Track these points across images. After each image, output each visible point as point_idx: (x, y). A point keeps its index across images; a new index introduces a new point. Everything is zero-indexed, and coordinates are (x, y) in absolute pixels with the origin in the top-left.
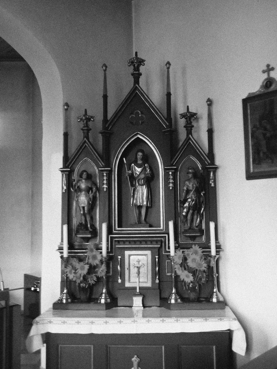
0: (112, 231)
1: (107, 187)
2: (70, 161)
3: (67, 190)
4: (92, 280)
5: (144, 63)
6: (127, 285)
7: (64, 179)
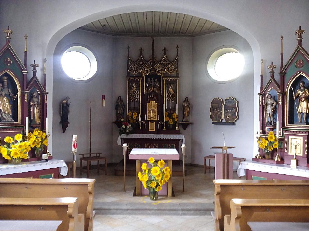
0: (285, 126)
1: (281, 103)
2: (263, 89)
3: (282, 104)
4: (271, 149)
5: (304, 32)
6: (290, 154)
7: (260, 99)
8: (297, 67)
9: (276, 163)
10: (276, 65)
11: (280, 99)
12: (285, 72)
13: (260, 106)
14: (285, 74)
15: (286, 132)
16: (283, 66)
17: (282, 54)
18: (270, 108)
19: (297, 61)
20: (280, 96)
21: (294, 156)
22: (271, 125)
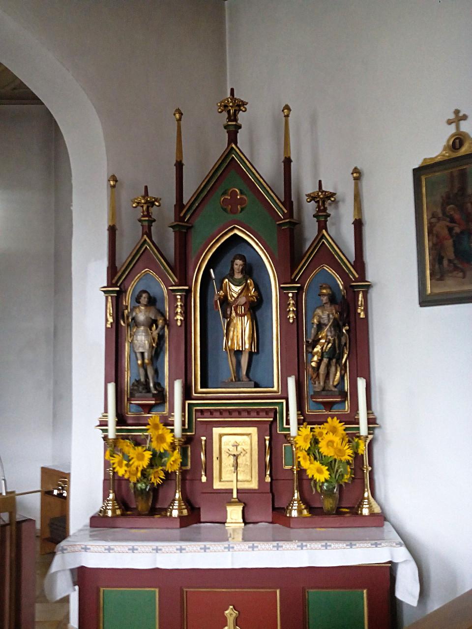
1: (182, 318)
5: (245, 108)
6: (217, 485)
7: (110, 305)
8: (225, 210)
9: (178, 526)
10: (160, 199)
11: (177, 306)
12: (190, 221)
13: (107, 328)
14: (189, 228)
15: (205, 414)
16: (185, 202)
17: (179, 166)
18: (147, 335)
19: (224, 193)
20: (179, 297)
21: (232, 493)
22: (151, 395)
